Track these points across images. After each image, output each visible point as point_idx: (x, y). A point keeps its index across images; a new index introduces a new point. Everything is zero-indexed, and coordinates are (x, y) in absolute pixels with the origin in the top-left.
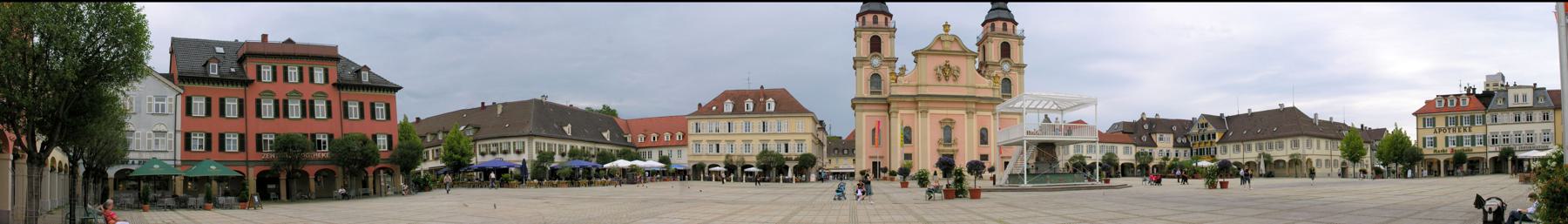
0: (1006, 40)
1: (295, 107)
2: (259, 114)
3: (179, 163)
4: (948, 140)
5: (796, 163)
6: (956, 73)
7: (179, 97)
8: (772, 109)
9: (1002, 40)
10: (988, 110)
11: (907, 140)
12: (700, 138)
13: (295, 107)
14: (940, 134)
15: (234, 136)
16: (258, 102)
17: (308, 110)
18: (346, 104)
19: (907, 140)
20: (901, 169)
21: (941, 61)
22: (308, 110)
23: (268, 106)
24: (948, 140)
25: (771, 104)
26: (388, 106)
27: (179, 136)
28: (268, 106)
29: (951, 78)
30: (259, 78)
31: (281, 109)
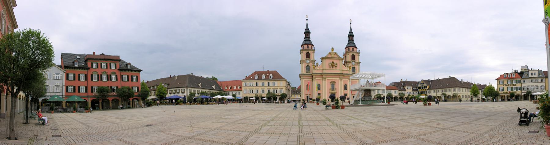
0: (353, 54)
1: (105, 77)
2: (92, 80)
3: (64, 96)
4: (333, 89)
5: (280, 97)
6: (336, 65)
7: (64, 74)
8: (272, 78)
9: (352, 54)
10: (338, 78)
11: (319, 88)
12: (257, 88)
13: (105, 77)
14: (330, 87)
15: (96, 87)
16: (92, 75)
17: (109, 78)
18: (122, 76)
19: (319, 88)
20: (317, 99)
21: (331, 61)
22: (109, 78)
23: (95, 77)
24: (333, 89)
25: (271, 76)
26: (137, 77)
27: (64, 87)
28: (95, 77)
29: (334, 67)
30: (92, 67)
31: (100, 78)
